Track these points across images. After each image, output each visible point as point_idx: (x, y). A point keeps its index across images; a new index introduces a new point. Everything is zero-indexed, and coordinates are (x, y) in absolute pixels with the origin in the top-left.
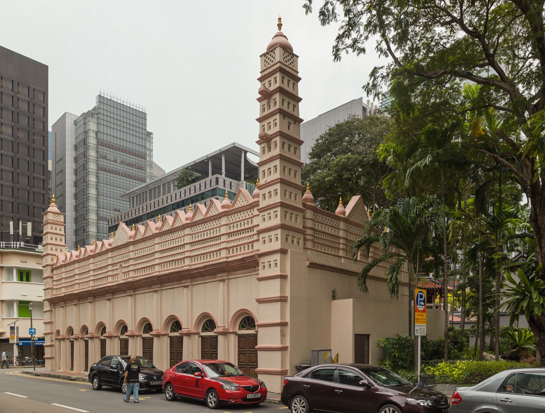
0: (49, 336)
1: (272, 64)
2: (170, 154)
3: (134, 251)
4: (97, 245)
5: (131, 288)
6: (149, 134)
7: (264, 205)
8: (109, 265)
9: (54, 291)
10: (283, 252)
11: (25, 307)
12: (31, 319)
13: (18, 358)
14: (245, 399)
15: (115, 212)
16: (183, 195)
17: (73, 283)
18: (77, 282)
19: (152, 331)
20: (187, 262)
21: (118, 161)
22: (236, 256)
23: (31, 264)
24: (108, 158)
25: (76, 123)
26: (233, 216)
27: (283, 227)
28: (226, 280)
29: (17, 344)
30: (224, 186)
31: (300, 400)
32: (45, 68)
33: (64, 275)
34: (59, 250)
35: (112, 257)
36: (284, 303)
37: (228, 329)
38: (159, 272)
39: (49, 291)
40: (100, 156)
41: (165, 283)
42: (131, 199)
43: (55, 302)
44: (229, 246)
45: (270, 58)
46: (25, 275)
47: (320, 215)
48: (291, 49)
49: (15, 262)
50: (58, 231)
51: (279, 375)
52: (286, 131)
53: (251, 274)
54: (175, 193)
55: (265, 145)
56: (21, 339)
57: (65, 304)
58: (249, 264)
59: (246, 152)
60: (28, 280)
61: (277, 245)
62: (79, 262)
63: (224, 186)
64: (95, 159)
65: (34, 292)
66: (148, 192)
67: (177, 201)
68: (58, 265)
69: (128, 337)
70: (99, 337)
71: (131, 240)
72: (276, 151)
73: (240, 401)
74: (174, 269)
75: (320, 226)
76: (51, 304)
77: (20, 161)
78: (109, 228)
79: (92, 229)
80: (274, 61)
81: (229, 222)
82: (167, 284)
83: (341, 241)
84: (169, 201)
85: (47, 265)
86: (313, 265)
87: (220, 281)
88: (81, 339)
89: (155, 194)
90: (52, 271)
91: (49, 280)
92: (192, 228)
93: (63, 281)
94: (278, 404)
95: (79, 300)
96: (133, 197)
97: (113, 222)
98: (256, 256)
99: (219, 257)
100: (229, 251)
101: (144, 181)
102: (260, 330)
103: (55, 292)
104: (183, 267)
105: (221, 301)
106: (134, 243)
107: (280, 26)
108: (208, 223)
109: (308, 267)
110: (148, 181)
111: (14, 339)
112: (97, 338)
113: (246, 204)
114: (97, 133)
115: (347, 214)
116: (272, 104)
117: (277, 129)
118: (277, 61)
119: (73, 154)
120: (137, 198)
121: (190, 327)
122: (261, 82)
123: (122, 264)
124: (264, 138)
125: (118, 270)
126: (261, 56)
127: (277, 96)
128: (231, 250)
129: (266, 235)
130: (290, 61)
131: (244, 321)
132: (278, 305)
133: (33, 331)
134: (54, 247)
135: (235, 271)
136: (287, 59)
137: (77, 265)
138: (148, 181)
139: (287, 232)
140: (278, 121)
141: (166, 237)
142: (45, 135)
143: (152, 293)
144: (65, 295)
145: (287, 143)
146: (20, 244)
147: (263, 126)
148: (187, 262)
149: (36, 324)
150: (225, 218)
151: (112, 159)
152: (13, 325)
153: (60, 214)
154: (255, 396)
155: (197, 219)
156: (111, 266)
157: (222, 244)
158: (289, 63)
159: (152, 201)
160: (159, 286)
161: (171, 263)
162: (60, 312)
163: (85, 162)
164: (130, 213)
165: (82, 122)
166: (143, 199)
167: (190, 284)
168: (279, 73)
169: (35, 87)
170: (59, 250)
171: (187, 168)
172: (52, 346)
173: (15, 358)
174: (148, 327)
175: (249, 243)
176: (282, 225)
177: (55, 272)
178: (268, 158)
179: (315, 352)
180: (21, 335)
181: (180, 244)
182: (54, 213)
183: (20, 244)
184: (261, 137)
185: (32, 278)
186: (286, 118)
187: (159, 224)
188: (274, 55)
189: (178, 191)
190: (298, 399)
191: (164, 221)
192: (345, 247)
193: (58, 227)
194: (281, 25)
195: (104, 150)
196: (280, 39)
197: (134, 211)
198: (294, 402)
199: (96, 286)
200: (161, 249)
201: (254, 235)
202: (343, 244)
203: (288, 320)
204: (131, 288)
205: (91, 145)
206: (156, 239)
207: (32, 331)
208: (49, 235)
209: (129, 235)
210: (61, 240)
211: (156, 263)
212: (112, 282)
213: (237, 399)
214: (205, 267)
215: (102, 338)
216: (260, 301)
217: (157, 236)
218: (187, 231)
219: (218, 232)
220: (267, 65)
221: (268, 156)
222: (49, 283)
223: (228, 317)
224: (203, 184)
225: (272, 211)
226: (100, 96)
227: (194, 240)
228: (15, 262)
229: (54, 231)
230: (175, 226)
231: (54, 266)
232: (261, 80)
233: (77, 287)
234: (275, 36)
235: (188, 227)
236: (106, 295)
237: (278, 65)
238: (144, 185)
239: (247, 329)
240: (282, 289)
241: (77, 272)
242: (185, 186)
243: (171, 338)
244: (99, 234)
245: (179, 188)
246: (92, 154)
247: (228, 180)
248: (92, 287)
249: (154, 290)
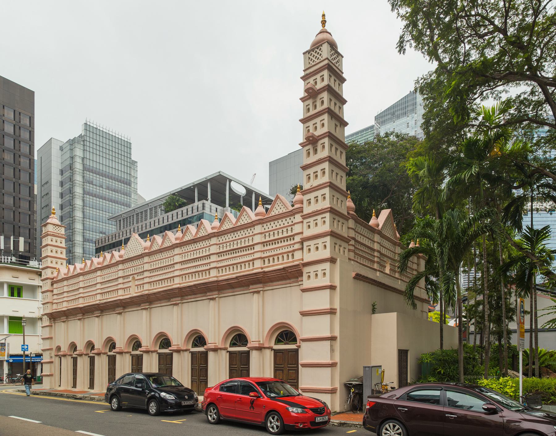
0: (48, 352)
2: (153, 183)
3: (149, 263)
4: (86, 264)
5: (102, 309)
6: (134, 163)
7: (310, 211)
8: (120, 277)
9: (54, 305)
10: (332, 260)
11: (16, 323)
12: (24, 336)
13: (9, 375)
14: (314, 423)
15: (101, 235)
16: (170, 219)
17: (77, 297)
18: (82, 295)
19: (115, 348)
20: (214, 273)
21: (104, 187)
22: (273, 266)
23: (23, 279)
24: (94, 183)
25: (61, 149)
26: (268, 224)
27: (333, 234)
28: (261, 292)
29: (7, 361)
30: (211, 212)
31: (394, 426)
32: (32, 93)
33: (66, 289)
34: (59, 263)
35: (123, 270)
36: (333, 316)
37: (263, 344)
38: (180, 284)
39: (49, 305)
40: (85, 181)
41: (187, 295)
42: (118, 222)
43: (54, 317)
44: (263, 256)
45: (316, 55)
46: (16, 291)
47: (360, 226)
48: (336, 47)
49: (7, 277)
50: (58, 244)
51: (329, 393)
52: (333, 132)
53: (292, 285)
54: (137, 225)
55: (310, 147)
56: (12, 356)
57: (67, 319)
58: (291, 275)
59: (230, 181)
60: (19, 295)
61: (326, 254)
62: (83, 275)
63: (211, 212)
64: (81, 183)
65: (28, 307)
66: (135, 216)
67: (165, 224)
68: (59, 278)
69: (142, 353)
70: (107, 353)
71: (147, 251)
72: (324, 153)
73: (308, 425)
74: (198, 280)
75: (359, 237)
76: (50, 319)
77: (5, 182)
78: (96, 249)
79: (78, 250)
80: (320, 58)
81: (263, 231)
82: (189, 297)
83: (376, 254)
84: (157, 224)
85: (47, 279)
86: (358, 277)
87: (254, 292)
88: (86, 355)
89: (142, 218)
90: (52, 285)
91: (48, 293)
92: (182, 247)
93: (65, 295)
94: (338, 426)
95: (84, 314)
96: (120, 221)
97: (100, 244)
98: (301, 266)
99: (142, 290)
100: (264, 261)
101: (129, 206)
102: (304, 345)
103: (55, 306)
104: (142, 291)
105: (256, 314)
106: (149, 254)
107: (324, 22)
108: (239, 232)
109: (354, 278)
110: (133, 206)
111: (4, 355)
112: (104, 354)
113: (284, 211)
114: (83, 159)
115: (380, 227)
116: (318, 103)
117: (325, 130)
118: (324, 58)
119: (59, 178)
120: (124, 221)
121: (217, 342)
122: (304, 80)
123: (135, 276)
124: (311, 138)
125: (130, 283)
126: (304, 54)
127: (325, 96)
128: (266, 260)
129: (312, 243)
130: (336, 60)
131: (281, 335)
132: (327, 317)
133: (26, 347)
134: (54, 260)
135: (272, 281)
137: (81, 278)
138: (133, 206)
139: (335, 240)
140: (326, 122)
141: (153, 257)
142: (31, 157)
143: (171, 306)
144: (68, 310)
145: (335, 146)
146: (11, 259)
147: (307, 128)
148: (214, 273)
149: (28, 341)
150: (260, 226)
151: (98, 184)
152: (3, 341)
153: (60, 226)
154: (323, 419)
155: (225, 228)
156: (122, 279)
157: (255, 254)
159: (140, 224)
160: (179, 298)
161: (163, 281)
162: (60, 327)
163: (71, 186)
164: (117, 235)
165: (69, 148)
166: (130, 223)
167: (217, 296)
168: (326, 70)
169: (20, 111)
170: (59, 263)
171: (174, 194)
172: (51, 362)
173: (5, 376)
174: (137, 344)
175: (285, 253)
176: (331, 232)
177: (55, 286)
178: (314, 160)
179: (367, 369)
180: (12, 352)
181: (204, 254)
182: (54, 225)
183: (11, 259)
184: (307, 138)
185: (24, 294)
186: (333, 119)
187: (101, 259)
188: (320, 52)
189: (165, 216)
190: (391, 424)
191: (153, 242)
192: (378, 260)
193: (59, 239)
194: (325, 21)
195: (88, 175)
196: (325, 36)
197: (121, 234)
198: (384, 428)
199: (103, 300)
200: (181, 260)
201: (294, 244)
202: (377, 257)
203: (337, 333)
204: (102, 309)
205: (77, 170)
206: (176, 249)
207: (24, 347)
208: (49, 248)
209: (143, 246)
210: (61, 253)
211: (145, 282)
212: (123, 296)
213: (304, 423)
214: (237, 277)
215: (110, 353)
216: (304, 314)
217: (177, 247)
218: (214, 240)
219: (207, 252)
220: (311, 62)
221: (313, 158)
222: (49, 297)
223: (263, 331)
224: (190, 210)
225: (319, 217)
226: (86, 124)
227: (221, 250)
228: (7, 277)
229: (54, 243)
230: (198, 236)
231: (55, 280)
232: (304, 78)
233: (81, 301)
234: (320, 33)
235: (215, 236)
236: (116, 309)
237: (326, 62)
238: (129, 209)
239: (285, 344)
240: (332, 301)
241: (81, 285)
242: (172, 210)
243: (160, 355)
244: (85, 255)
245: (166, 212)
246: (78, 178)
247: (214, 206)
248: (100, 300)
249: (174, 302)
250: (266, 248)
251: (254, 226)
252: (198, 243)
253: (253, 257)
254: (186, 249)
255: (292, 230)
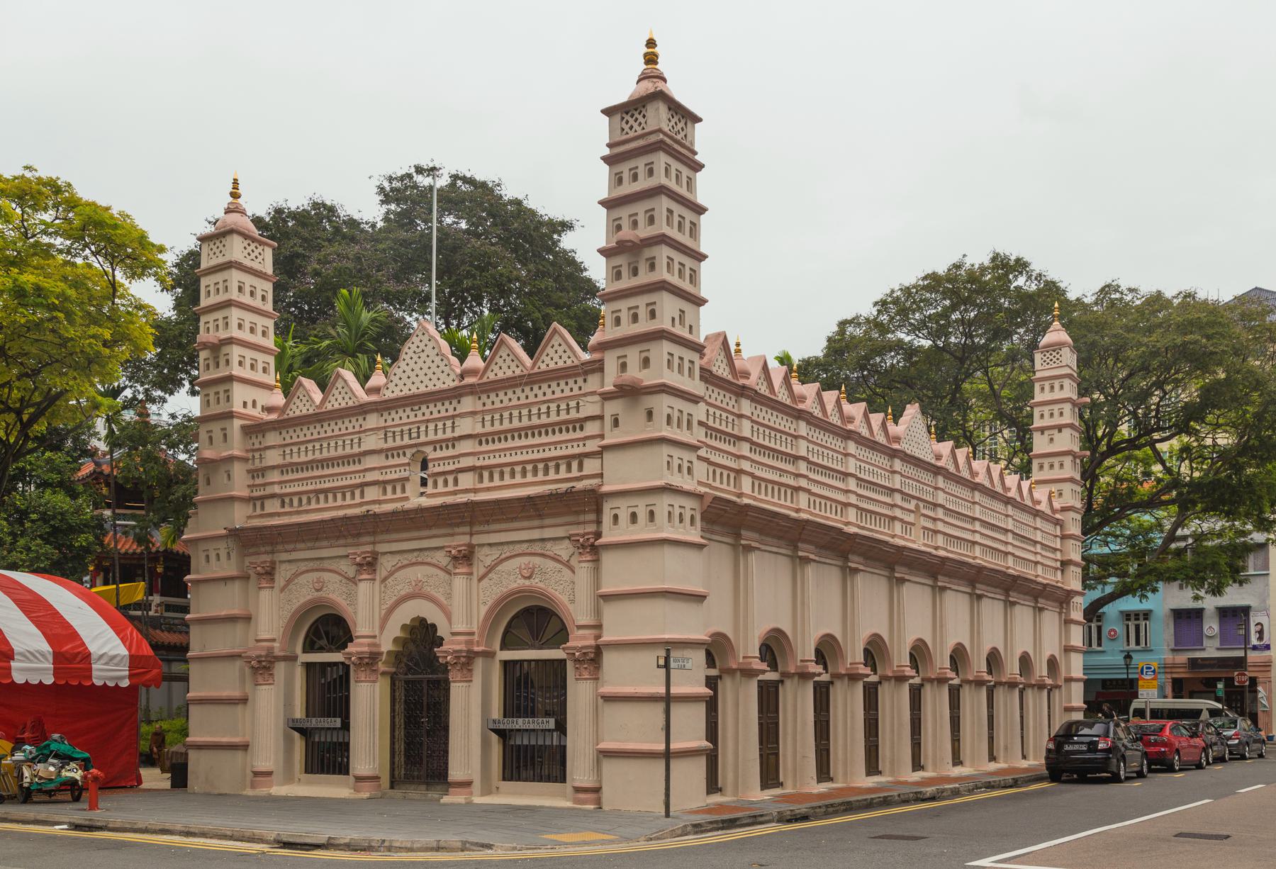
71: (469, 380)
250: (484, 448)
251: (366, 413)
252: (393, 412)
253: (262, 493)
254: (443, 409)
255: (453, 427)
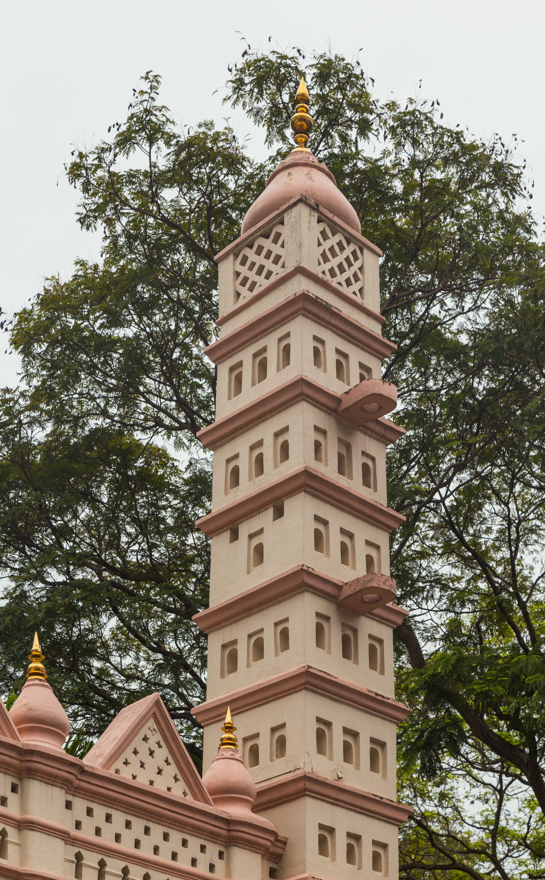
1: (263, 283)
45: (260, 260)
118: (290, 268)
130: (349, 273)
136: (334, 263)
158: (341, 278)
188: (276, 249)
